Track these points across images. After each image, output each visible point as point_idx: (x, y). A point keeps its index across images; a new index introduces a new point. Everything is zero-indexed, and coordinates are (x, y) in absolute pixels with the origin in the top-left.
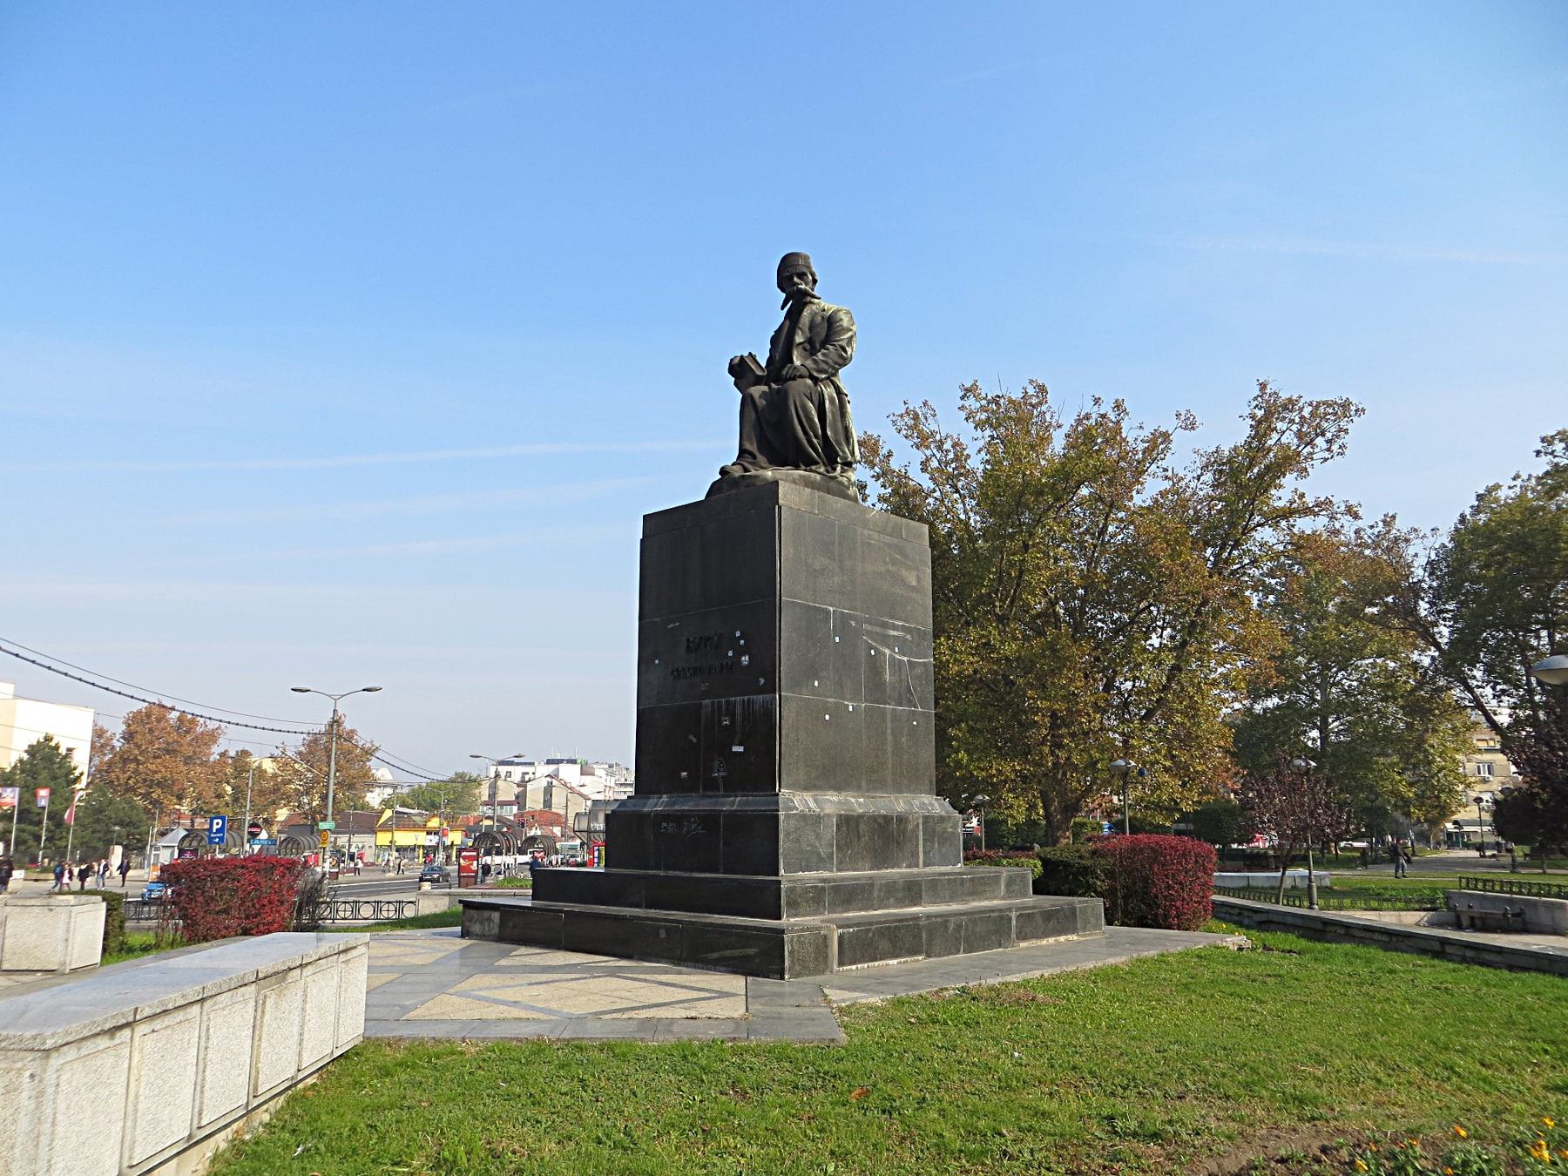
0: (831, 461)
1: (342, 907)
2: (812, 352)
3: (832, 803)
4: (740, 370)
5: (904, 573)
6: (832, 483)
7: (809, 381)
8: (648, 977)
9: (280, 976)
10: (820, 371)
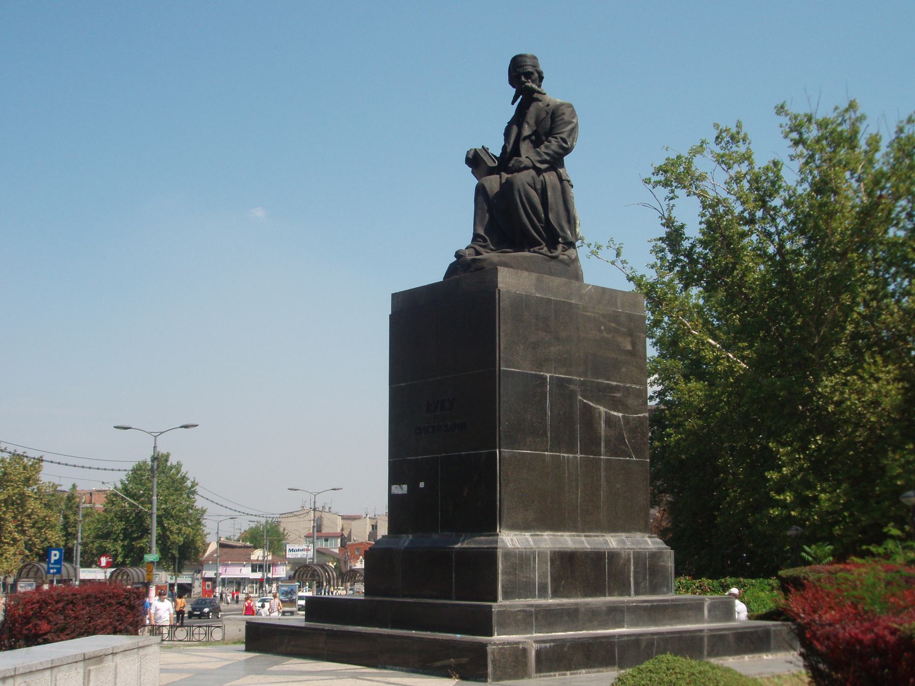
0: (552, 245)
1: (197, 631)
2: (536, 144)
3: (549, 541)
4: (475, 161)
5: (620, 339)
6: (553, 263)
7: (532, 172)
8: (377, 679)
9: (98, 658)
10: (542, 162)
